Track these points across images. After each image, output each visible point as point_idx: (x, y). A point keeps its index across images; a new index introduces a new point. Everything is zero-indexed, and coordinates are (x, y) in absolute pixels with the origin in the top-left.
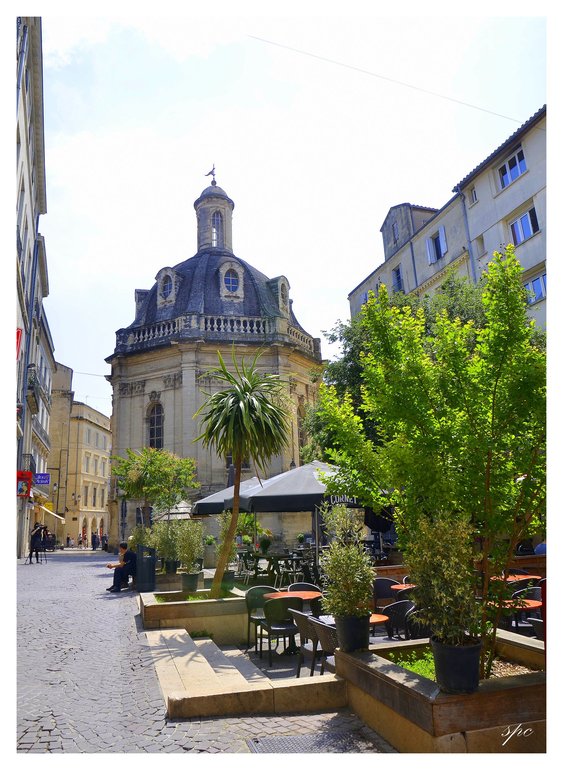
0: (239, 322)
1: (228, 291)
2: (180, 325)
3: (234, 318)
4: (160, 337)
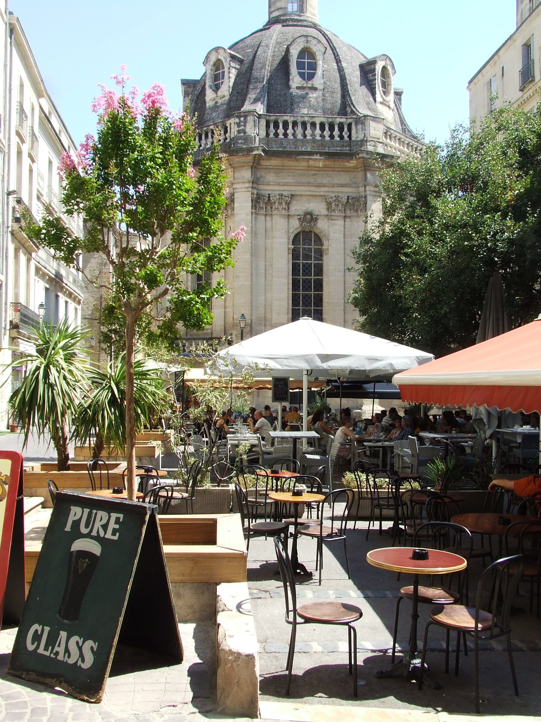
0: (313, 125)
1: (301, 79)
2: (233, 130)
3: (306, 119)
4: (208, 147)
